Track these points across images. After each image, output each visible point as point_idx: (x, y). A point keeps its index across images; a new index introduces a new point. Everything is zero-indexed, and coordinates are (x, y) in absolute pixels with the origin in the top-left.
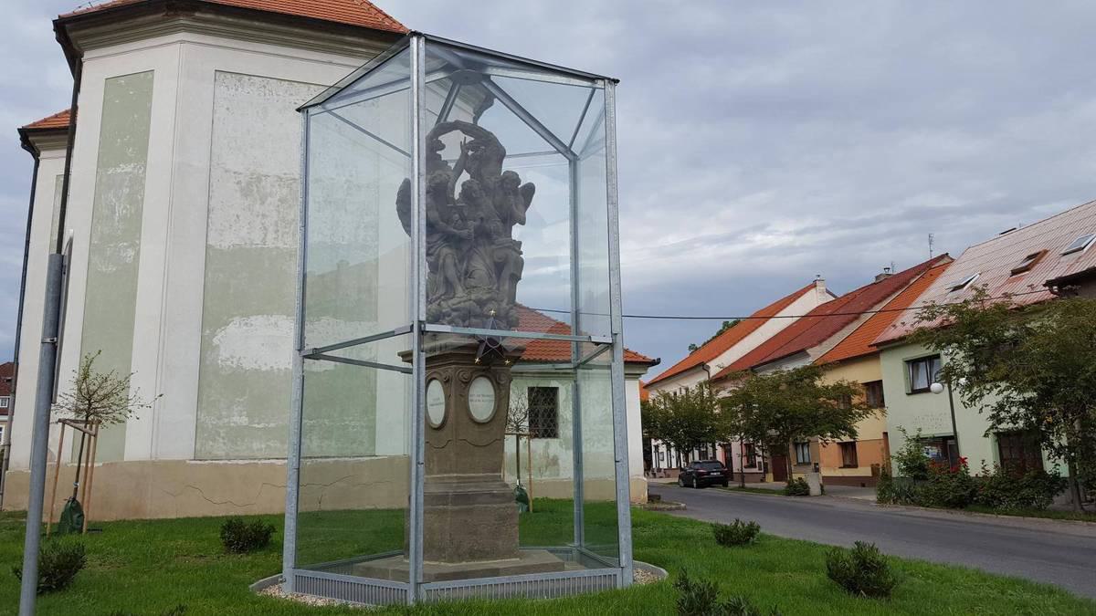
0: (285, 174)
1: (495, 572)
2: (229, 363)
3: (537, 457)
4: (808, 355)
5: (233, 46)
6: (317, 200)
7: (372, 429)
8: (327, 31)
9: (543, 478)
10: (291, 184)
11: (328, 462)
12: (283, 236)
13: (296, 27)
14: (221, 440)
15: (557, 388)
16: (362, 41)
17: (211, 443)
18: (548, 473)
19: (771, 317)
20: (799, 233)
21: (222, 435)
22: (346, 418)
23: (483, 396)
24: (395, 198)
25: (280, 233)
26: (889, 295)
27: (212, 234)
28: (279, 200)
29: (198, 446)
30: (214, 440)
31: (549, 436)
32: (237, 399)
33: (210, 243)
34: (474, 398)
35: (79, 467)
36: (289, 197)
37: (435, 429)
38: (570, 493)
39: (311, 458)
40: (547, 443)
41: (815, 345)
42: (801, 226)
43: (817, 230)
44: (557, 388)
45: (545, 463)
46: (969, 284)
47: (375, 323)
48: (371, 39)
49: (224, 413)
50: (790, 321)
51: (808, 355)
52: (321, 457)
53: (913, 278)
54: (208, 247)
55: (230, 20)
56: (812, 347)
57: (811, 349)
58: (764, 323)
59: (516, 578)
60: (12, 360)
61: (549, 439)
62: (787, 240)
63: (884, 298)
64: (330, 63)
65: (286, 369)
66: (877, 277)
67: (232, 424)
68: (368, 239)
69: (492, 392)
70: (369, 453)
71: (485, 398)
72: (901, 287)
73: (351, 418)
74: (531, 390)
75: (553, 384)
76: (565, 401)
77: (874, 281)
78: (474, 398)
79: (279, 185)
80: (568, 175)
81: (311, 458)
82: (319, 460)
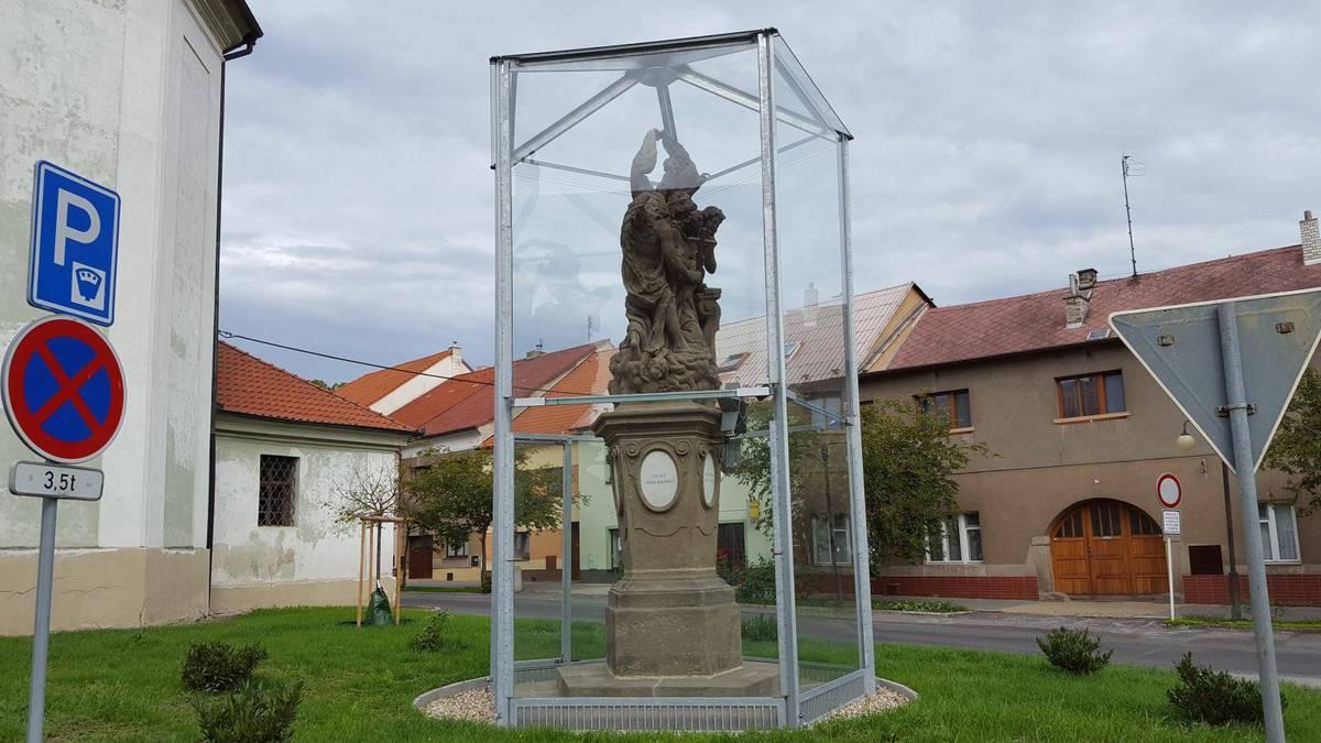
1: (645, 692)
3: (268, 552)
4: (479, 434)
9: (274, 580)
11: (24, 556)
15: (296, 459)
18: (280, 574)
19: (452, 379)
20: (301, 252)
24: (624, 301)
26: (557, 376)
35: (361, 581)
38: (356, 604)
40: (281, 533)
41: (487, 423)
42: (287, 244)
43: (328, 253)
44: (292, 461)
45: (277, 559)
50: (435, 383)
51: (479, 434)
52: (13, 548)
53: (579, 360)
56: (482, 425)
57: (375, 405)
58: (410, 379)
59: (599, 701)
62: (285, 260)
63: (553, 379)
66: (529, 354)
72: (568, 368)
74: (264, 458)
75: (293, 452)
76: (308, 475)
77: (525, 357)
82: (10, 552)
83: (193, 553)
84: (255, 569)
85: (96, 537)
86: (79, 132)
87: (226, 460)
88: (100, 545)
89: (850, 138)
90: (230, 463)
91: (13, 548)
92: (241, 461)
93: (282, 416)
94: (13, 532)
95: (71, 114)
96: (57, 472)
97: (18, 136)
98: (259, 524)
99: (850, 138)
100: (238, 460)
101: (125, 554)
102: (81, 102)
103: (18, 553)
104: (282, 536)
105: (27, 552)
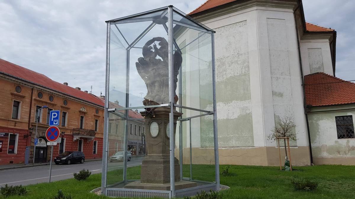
0: (219, 58)
2: (208, 118)
3: (343, 147)
5: (226, 17)
6: (229, 63)
7: (252, 137)
8: (205, 14)
10: (221, 60)
12: (219, 77)
13: (217, 10)
14: (207, 142)
16: (238, 5)
17: (205, 143)
18: (349, 154)
21: (207, 140)
22: (243, 134)
23: (155, 128)
25: (218, 77)
27: (201, 81)
28: (218, 66)
29: (202, 143)
30: (206, 142)
31: (350, 137)
32: (211, 129)
33: (200, 84)
34: (152, 129)
36: (220, 65)
37: (153, 137)
39: (233, 147)
45: (347, 149)
46: (170, 83)
47: (250, 100)
48: (241, 3)
49: (208, 133)
52: (236, 147)
54: (200, 85)
55: (200, 17)
60: (308, 116)
61: (350, 139)
64: (230, 17)
65: (223, 119)
67: (210, 137)
68: (246, 71)
69: (158, 127)
70: (252, 146)
71: (155, 129)
73: (245, 134)
74: (336, 117)
75: (349, 114)
78: (152, 129)
79: (217, 62)
80: (215, 49)
81: (233, 147)
82: (235, 148)
83: (297, 147)
84: (339, 152)
85: (254, 145)
86: (240, 56)
87: (322, 120)
88: (255, 146)
89: (215, 32)
90: (324, 120)
91: (236, 147)
92: (328, 119)
93: (336, 104)
94: (236, 144)
95: (238, 54)
96: (52, 143)
97: (228, 64)
98: (338, 138)
99: (215, 32)
100: (326, 119)
101: (260, 148)
102: (240, 50)
103: (237, 148)
104: (348, 142)
105: (238, 148)
